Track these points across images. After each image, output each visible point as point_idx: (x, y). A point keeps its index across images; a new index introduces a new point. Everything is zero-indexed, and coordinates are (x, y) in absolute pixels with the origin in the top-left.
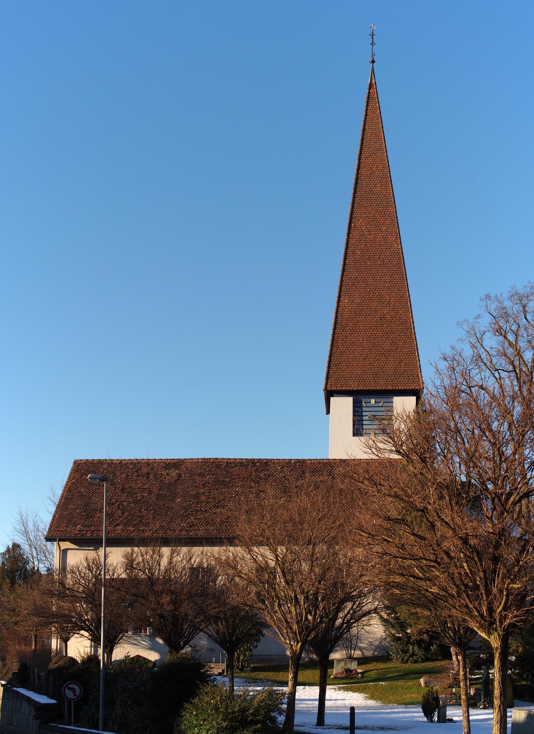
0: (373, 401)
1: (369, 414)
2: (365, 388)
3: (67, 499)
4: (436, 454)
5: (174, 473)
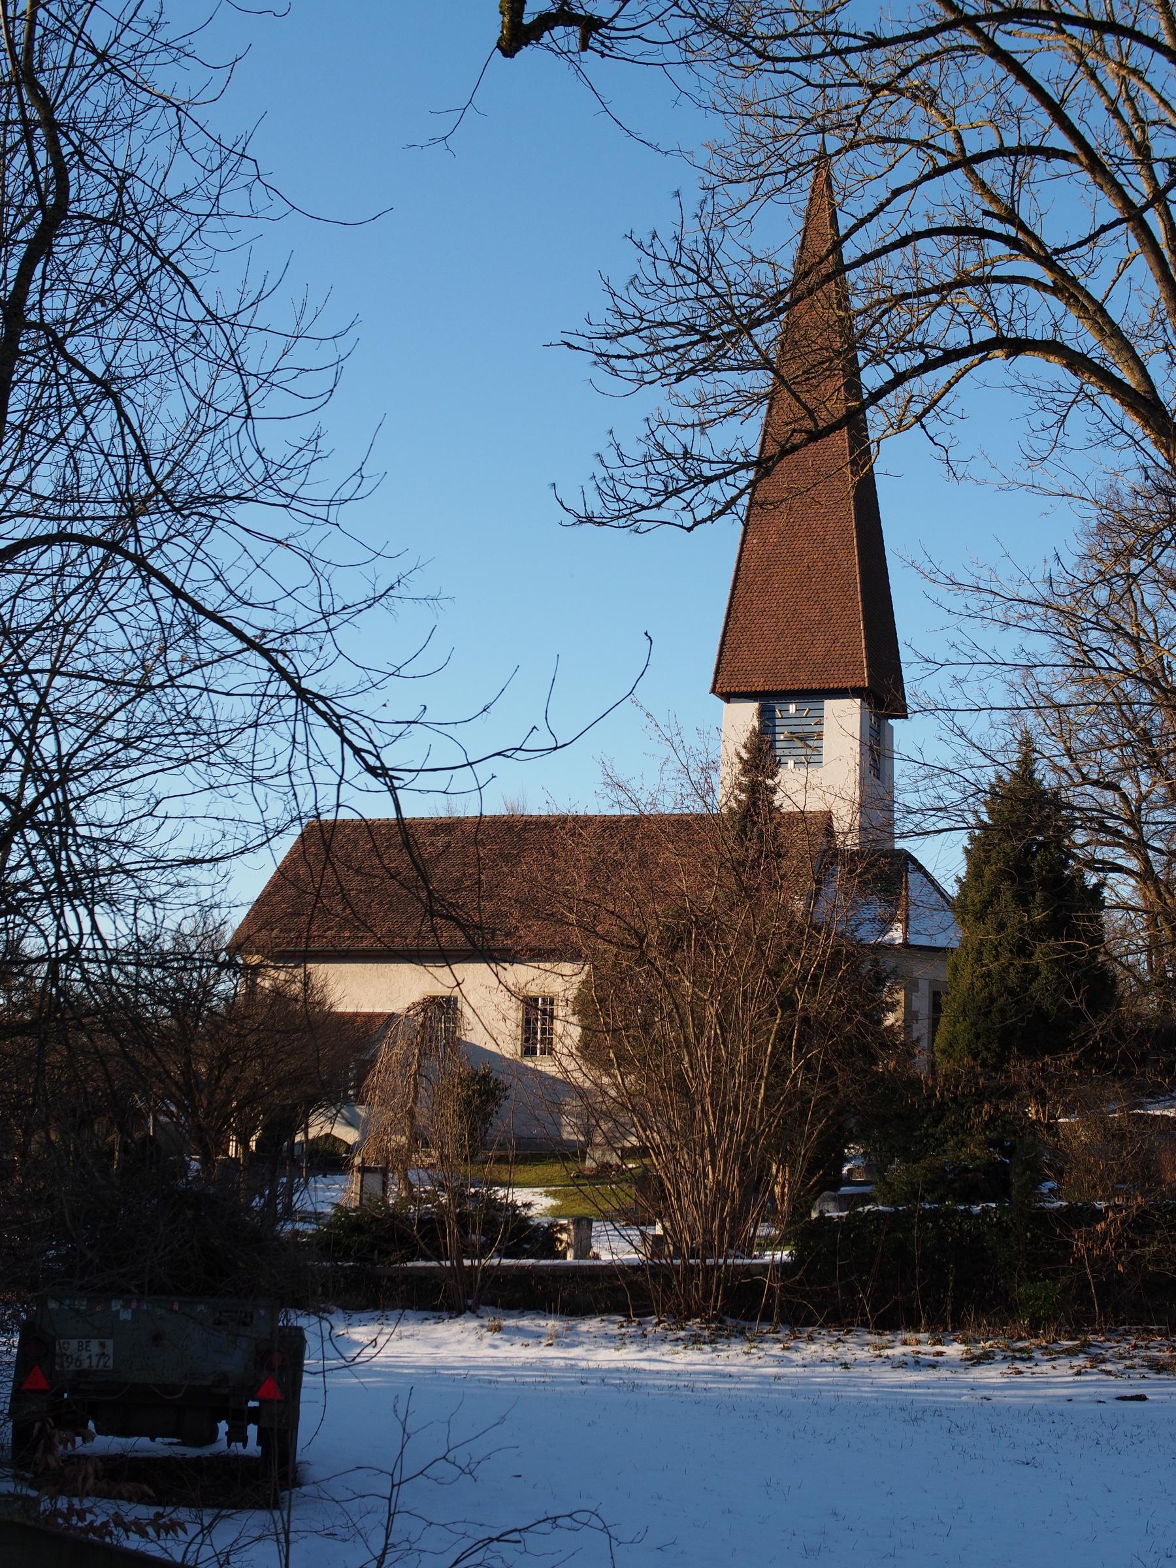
0: (792, 708)
1: (786, 730)
2: (775, 688)
3: (276, 885)
4: (71, 831)
5: (440, 841)
